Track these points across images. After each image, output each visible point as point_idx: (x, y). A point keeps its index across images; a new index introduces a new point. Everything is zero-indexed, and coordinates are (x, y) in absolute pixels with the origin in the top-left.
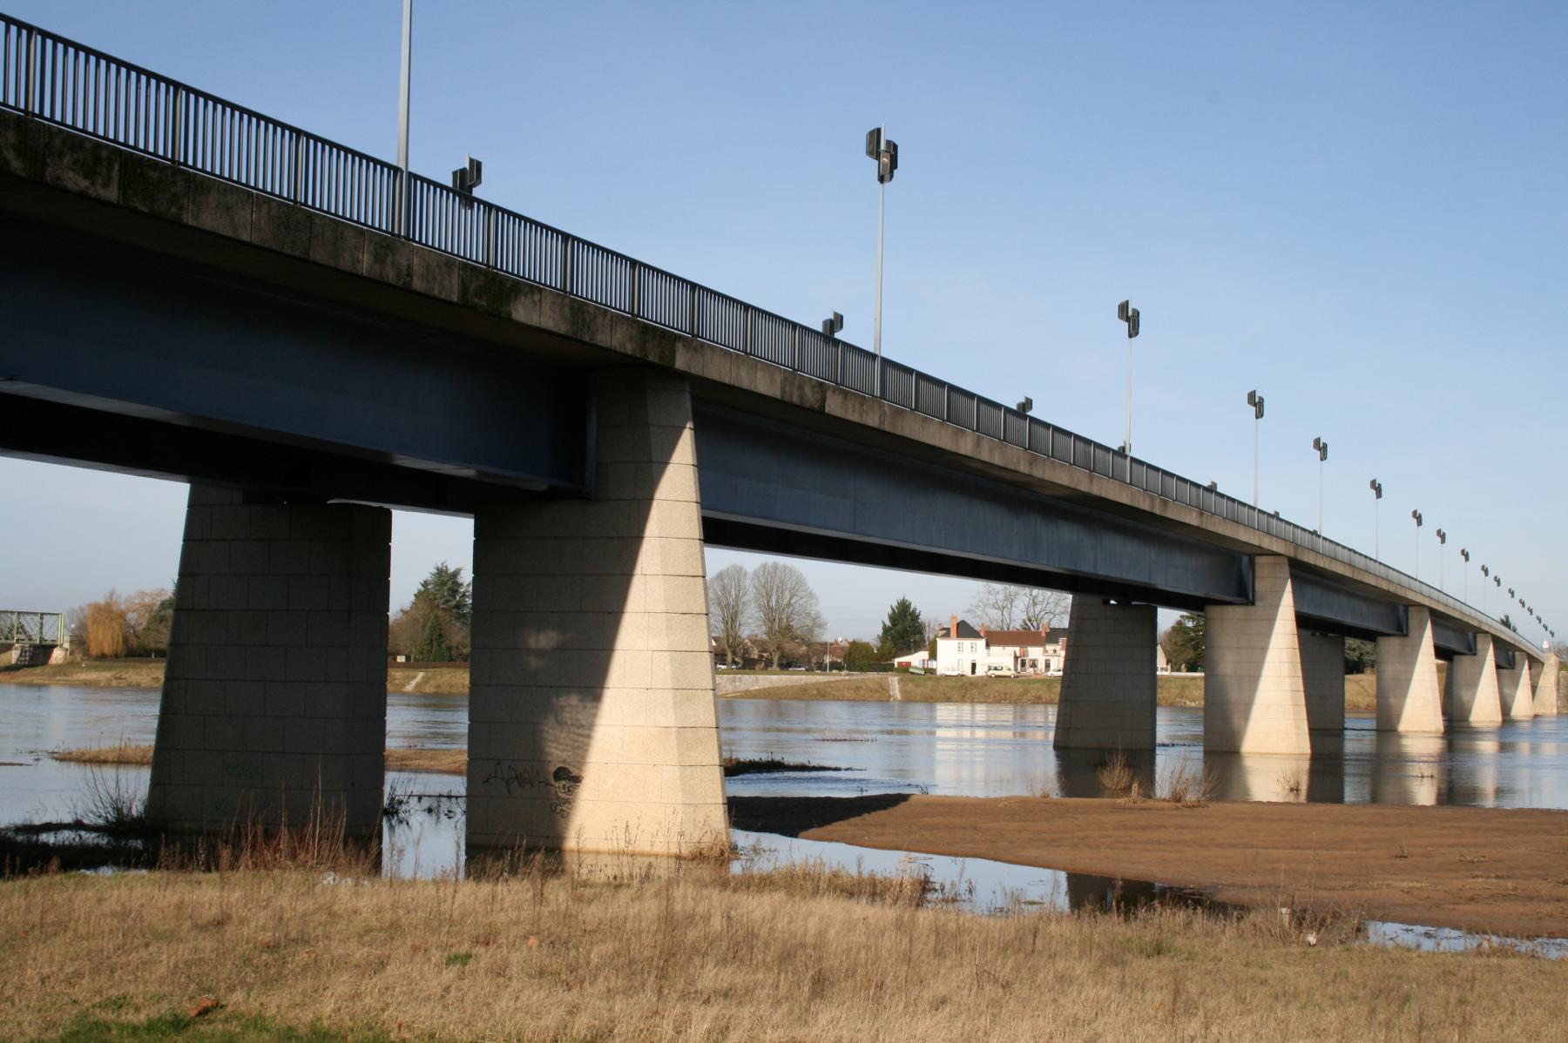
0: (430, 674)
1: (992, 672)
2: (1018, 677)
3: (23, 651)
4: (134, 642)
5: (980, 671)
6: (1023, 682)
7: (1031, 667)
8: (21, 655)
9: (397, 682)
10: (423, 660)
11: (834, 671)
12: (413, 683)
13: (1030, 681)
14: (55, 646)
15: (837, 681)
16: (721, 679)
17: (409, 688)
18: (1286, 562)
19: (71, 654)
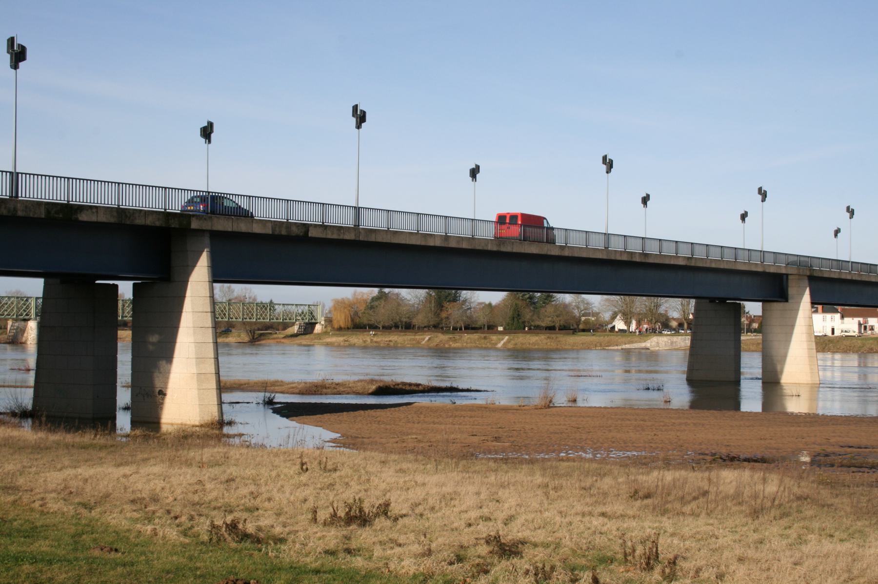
0: (512, 337)
1: (843, 333)
2: (860, 336)
3: (300, 326)
4: (357, 320)
5: (837, 333)
6: (863, 339)
7: (870, 330)
8: (299, 328)
9: (493, 342)
10: (508, 329)
11: (749, 334)
12: (502, 342)
13: (868, 339)
14: (317, 323)
15: (748, 339)
16: (678, 338)
17: (500, 345)
18: (806, 278)
19: (325, 327)
